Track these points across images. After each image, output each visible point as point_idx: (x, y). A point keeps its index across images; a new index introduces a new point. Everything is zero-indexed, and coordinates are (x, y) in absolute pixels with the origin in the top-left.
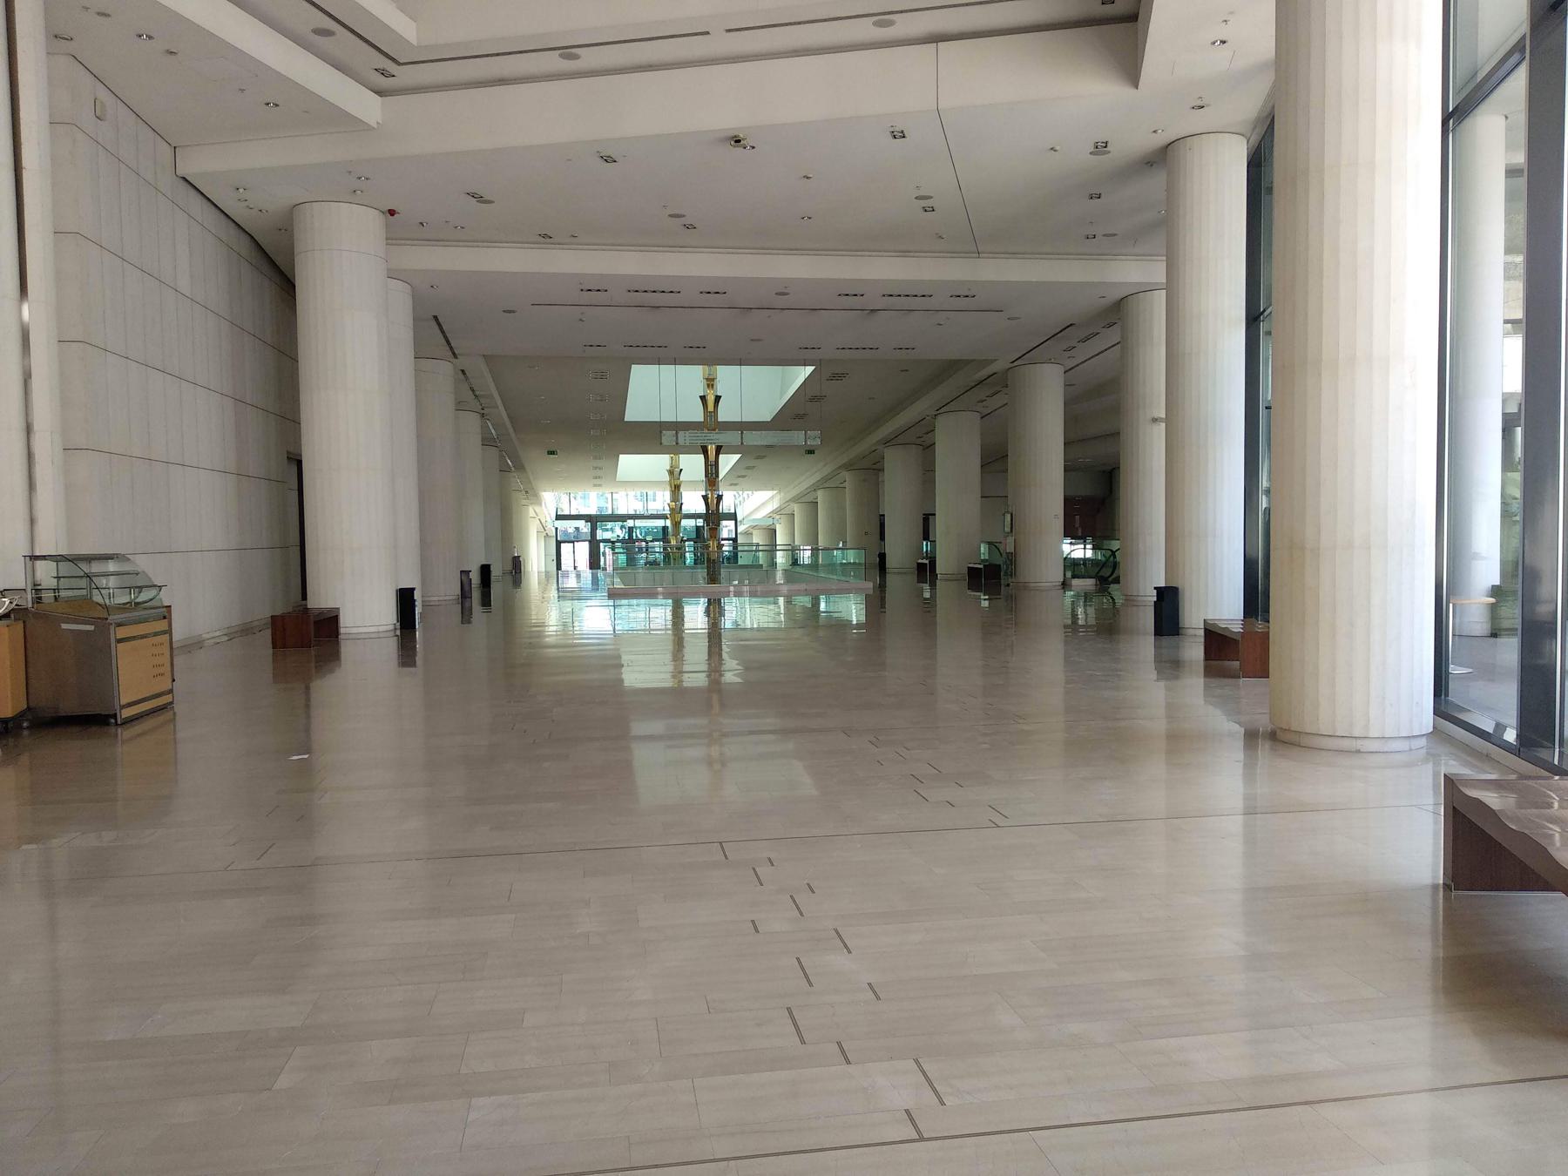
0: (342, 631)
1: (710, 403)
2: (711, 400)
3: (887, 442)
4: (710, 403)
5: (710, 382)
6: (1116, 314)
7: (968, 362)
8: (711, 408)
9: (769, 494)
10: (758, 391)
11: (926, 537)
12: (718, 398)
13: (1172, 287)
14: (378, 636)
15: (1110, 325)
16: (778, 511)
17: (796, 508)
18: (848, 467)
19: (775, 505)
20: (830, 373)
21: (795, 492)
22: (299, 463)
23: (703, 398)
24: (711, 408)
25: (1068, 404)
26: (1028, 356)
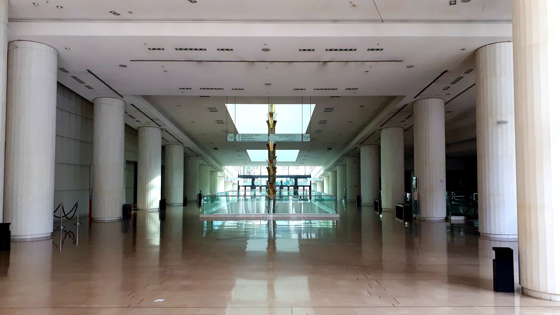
0: (11, 237)
1: (272, 126)
2: (271, 122)
3: (361, 143)
4: (272, 126)
5: (271, 114)
6: (471, 64)
7: (396, 97)
8: (271, 127)
9: (321, 167)
10: (295, 119)
11: (410, 191)
12: (275, 122)
13: (516, 40)
14: (112, 222)
15: (468, 72)
16: (323, 175)
17: (330, 174)
18: (347, 155)
19: (322, 172)
20: (326, 105)
21: (329, 166)
22: (136, 164)
23: (268, 122)
24: (271, 127)
25: (447, 124)
26: (422, 93)
